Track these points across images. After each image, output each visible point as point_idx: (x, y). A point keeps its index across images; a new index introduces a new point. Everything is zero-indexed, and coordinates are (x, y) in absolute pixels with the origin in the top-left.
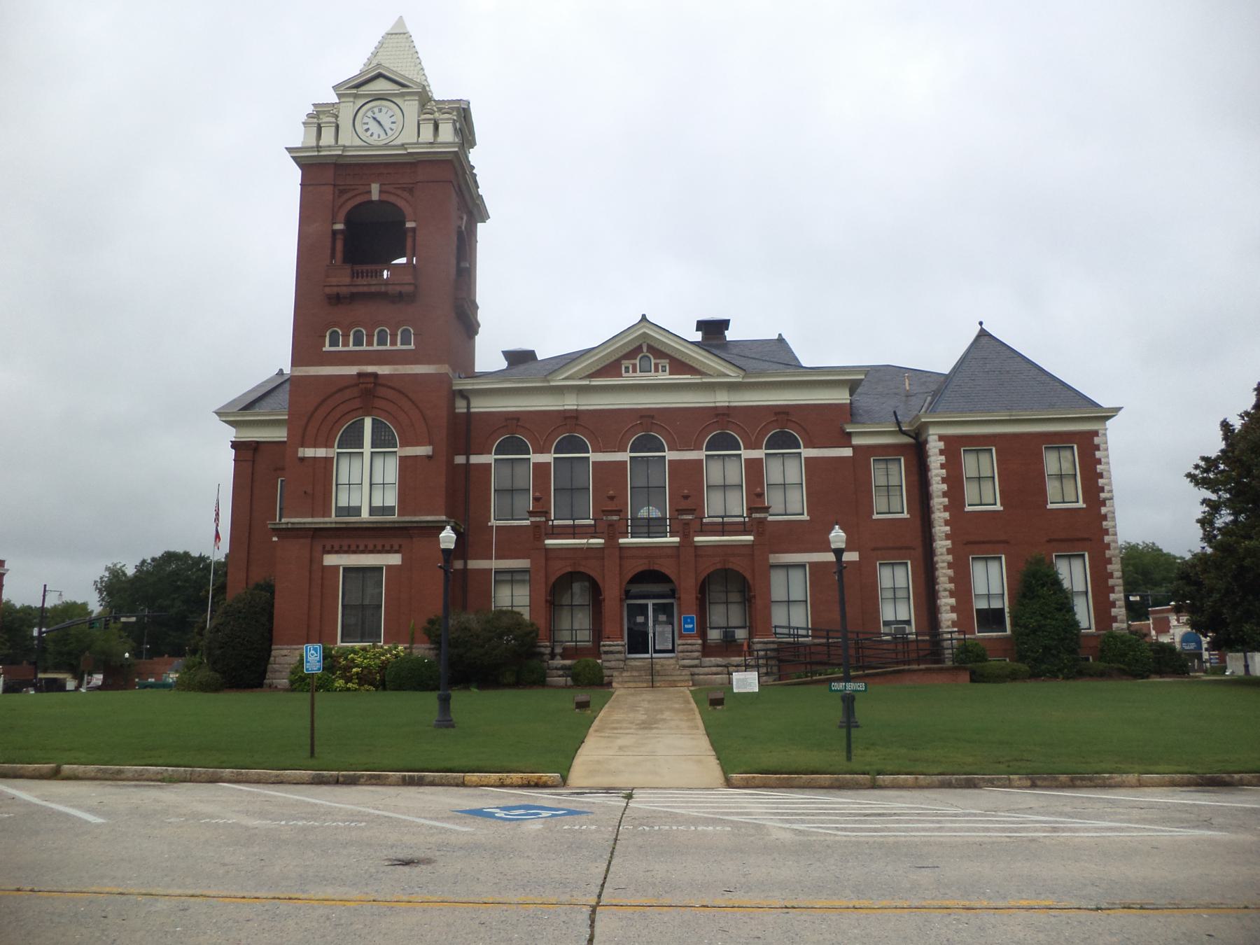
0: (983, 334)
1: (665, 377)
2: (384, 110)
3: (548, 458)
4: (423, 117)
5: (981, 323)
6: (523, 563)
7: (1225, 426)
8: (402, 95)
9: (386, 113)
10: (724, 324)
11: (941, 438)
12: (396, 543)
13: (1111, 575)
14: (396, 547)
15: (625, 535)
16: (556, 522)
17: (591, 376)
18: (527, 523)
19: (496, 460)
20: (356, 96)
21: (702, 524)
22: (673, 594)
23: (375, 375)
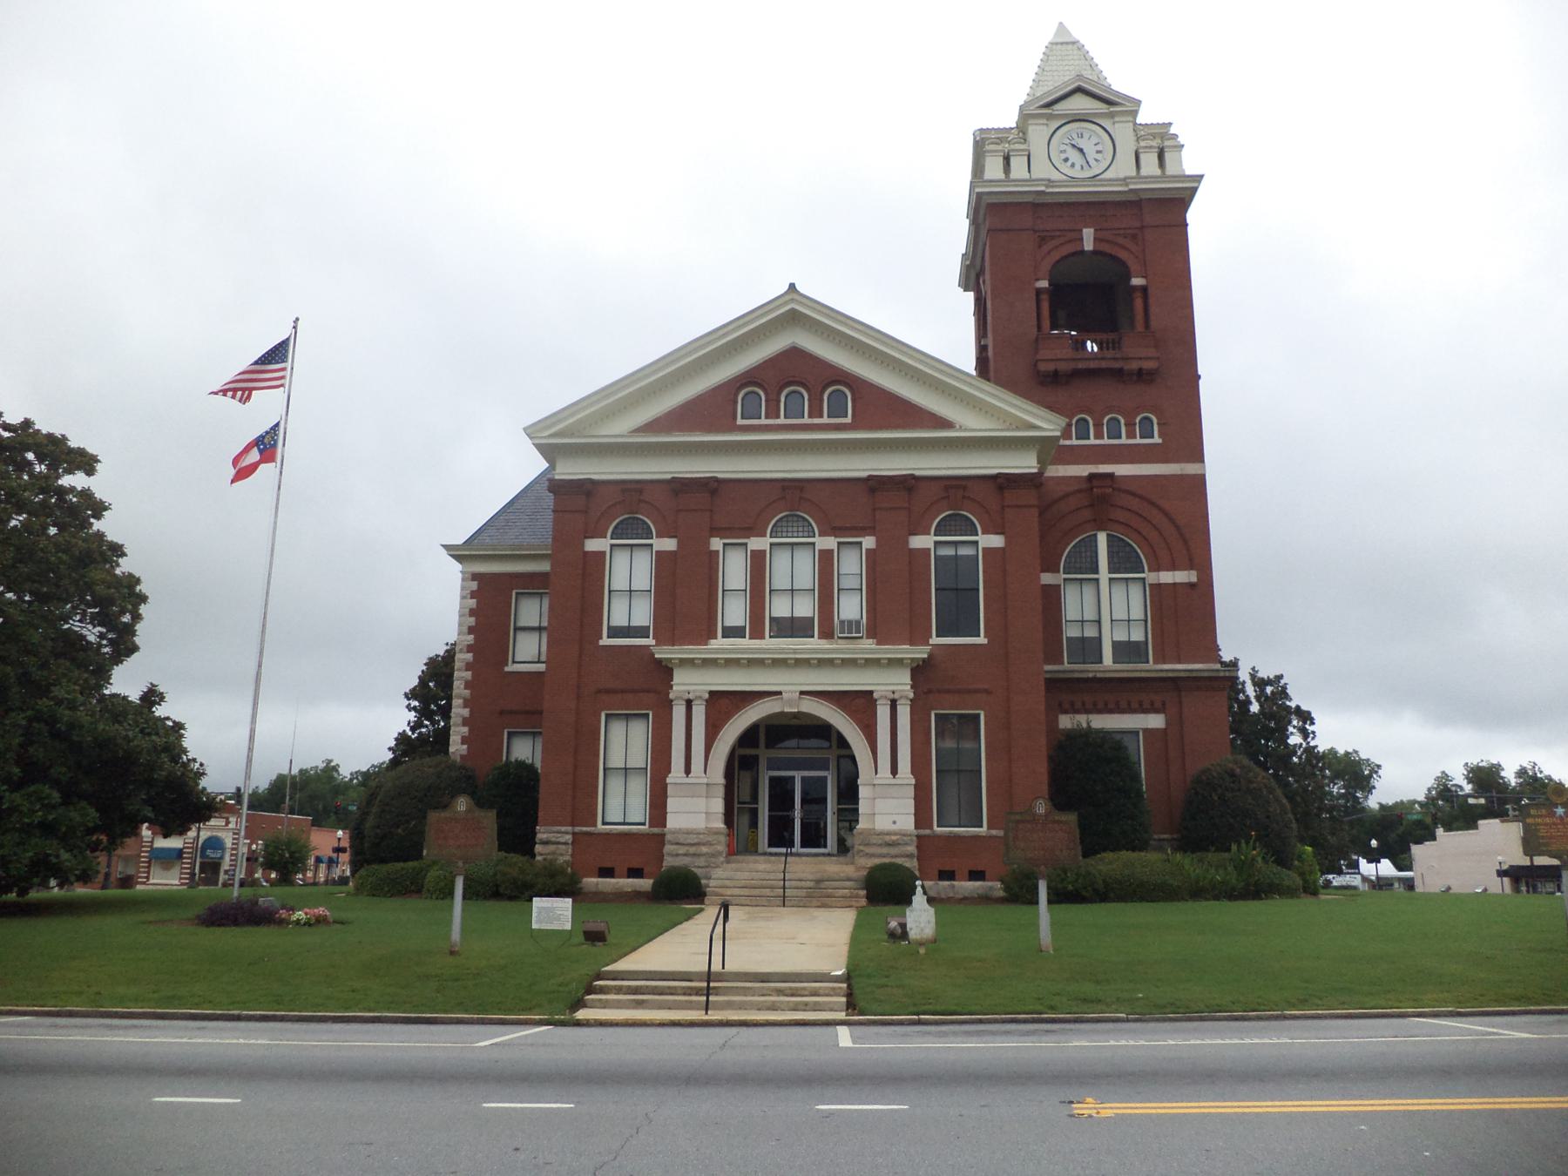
2: (1086, 136)
4: (1143, 144)
8: (1112, 115)
9: (1091, 139)
13: (468, 685)
14: (1158, 704)
19: (936, 543)
20: (1050, 117)
23: (1111, 476)
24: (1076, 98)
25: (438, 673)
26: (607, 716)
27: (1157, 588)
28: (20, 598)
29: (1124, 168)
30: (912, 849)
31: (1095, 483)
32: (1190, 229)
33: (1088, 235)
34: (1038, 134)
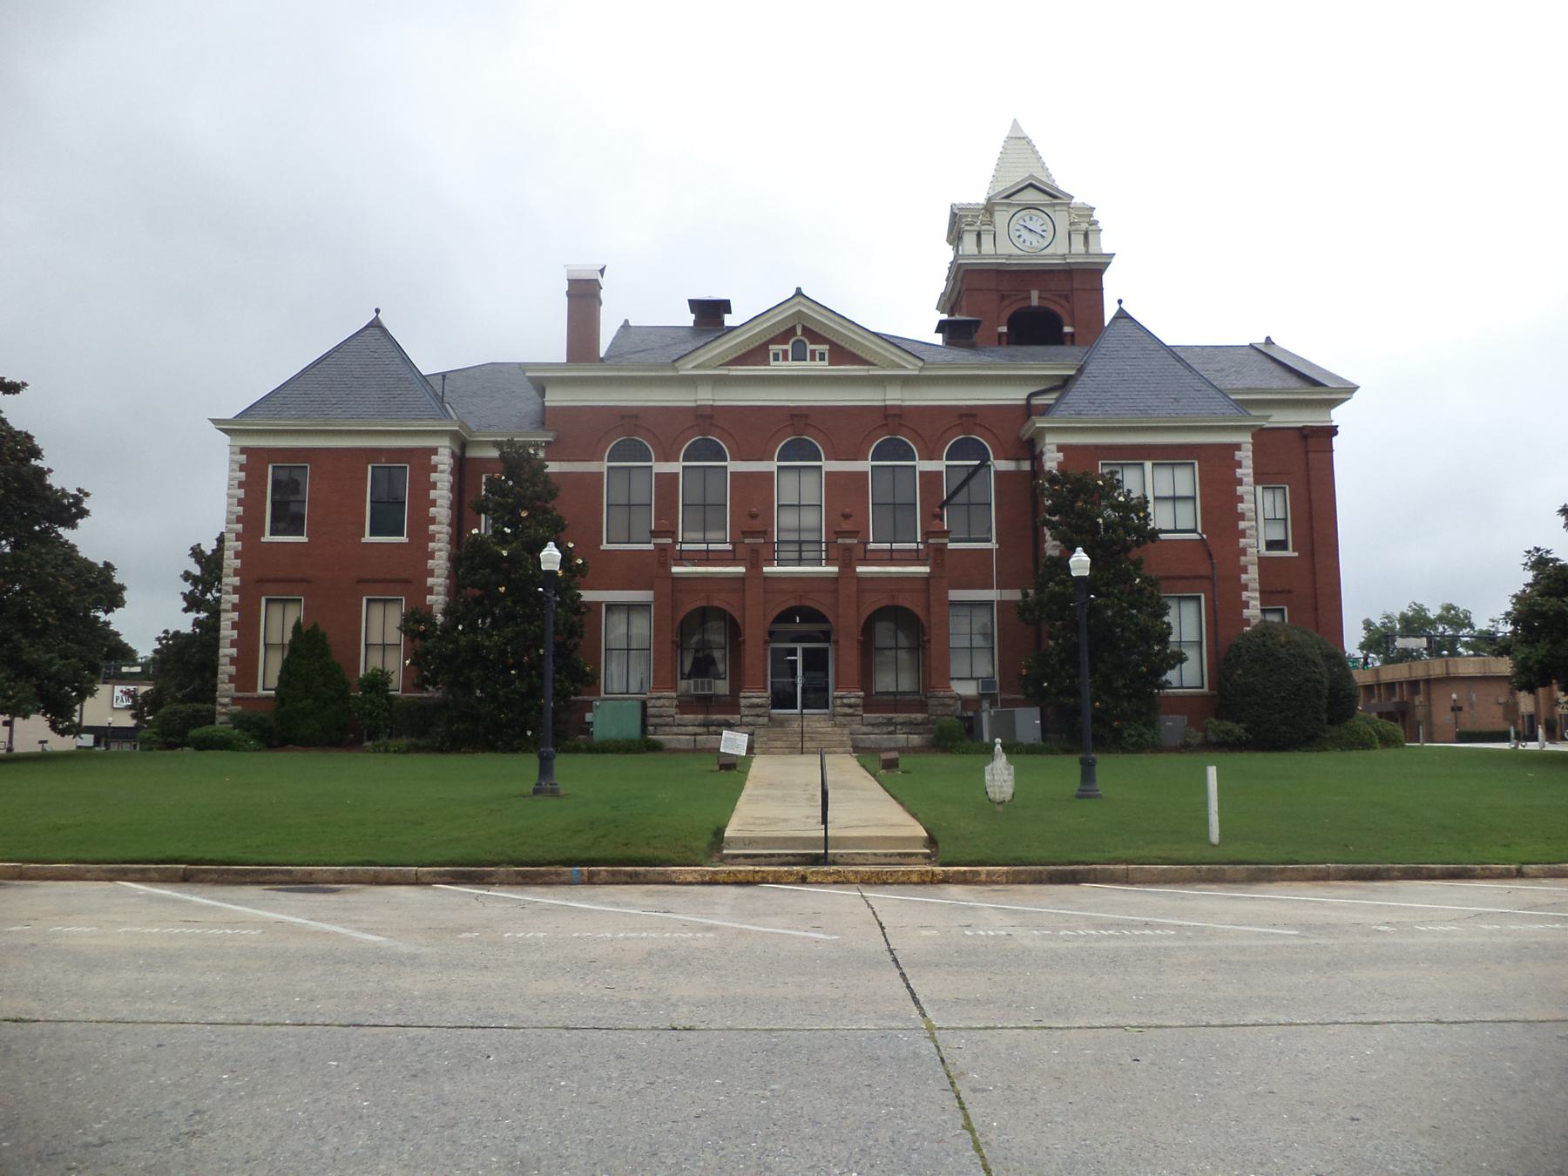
0: (376, 325)
1: (822, 367)
3: (676, 467)
5: (1120, 302)
6: (644, 596)
8: (1053, 205)
9: (1037, 222)
10: (724, 306)
11: (1060, 448)
15: (770, 563)
16: (685, 547)
17: (741, 360)
18: (651, 547)
19: (609, 468)
21: (866, 551)
22: (826, 636)
24: (1034, 193)
25: (209, 565)
26: (368, 601)
28: (506, 481)
29: (1060, 247)
33: (1035, 295)
34: (1001, 217)
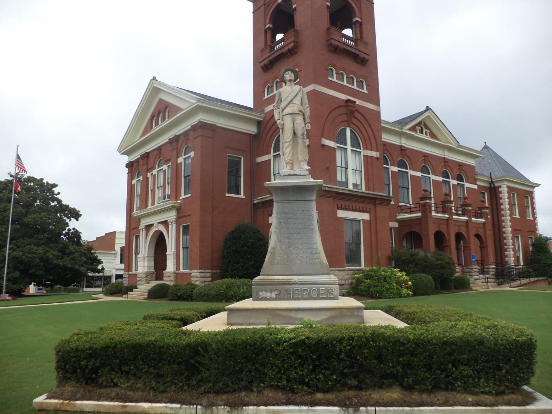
5: (485, 143)
7: (55, 186)
12: (368, 206)
16: (411, 203)
19: (273, 156)
23: (355, 102)
27: (366, 157)
30: (172, 278)
31: (349, 104)
32: (376, 7)
